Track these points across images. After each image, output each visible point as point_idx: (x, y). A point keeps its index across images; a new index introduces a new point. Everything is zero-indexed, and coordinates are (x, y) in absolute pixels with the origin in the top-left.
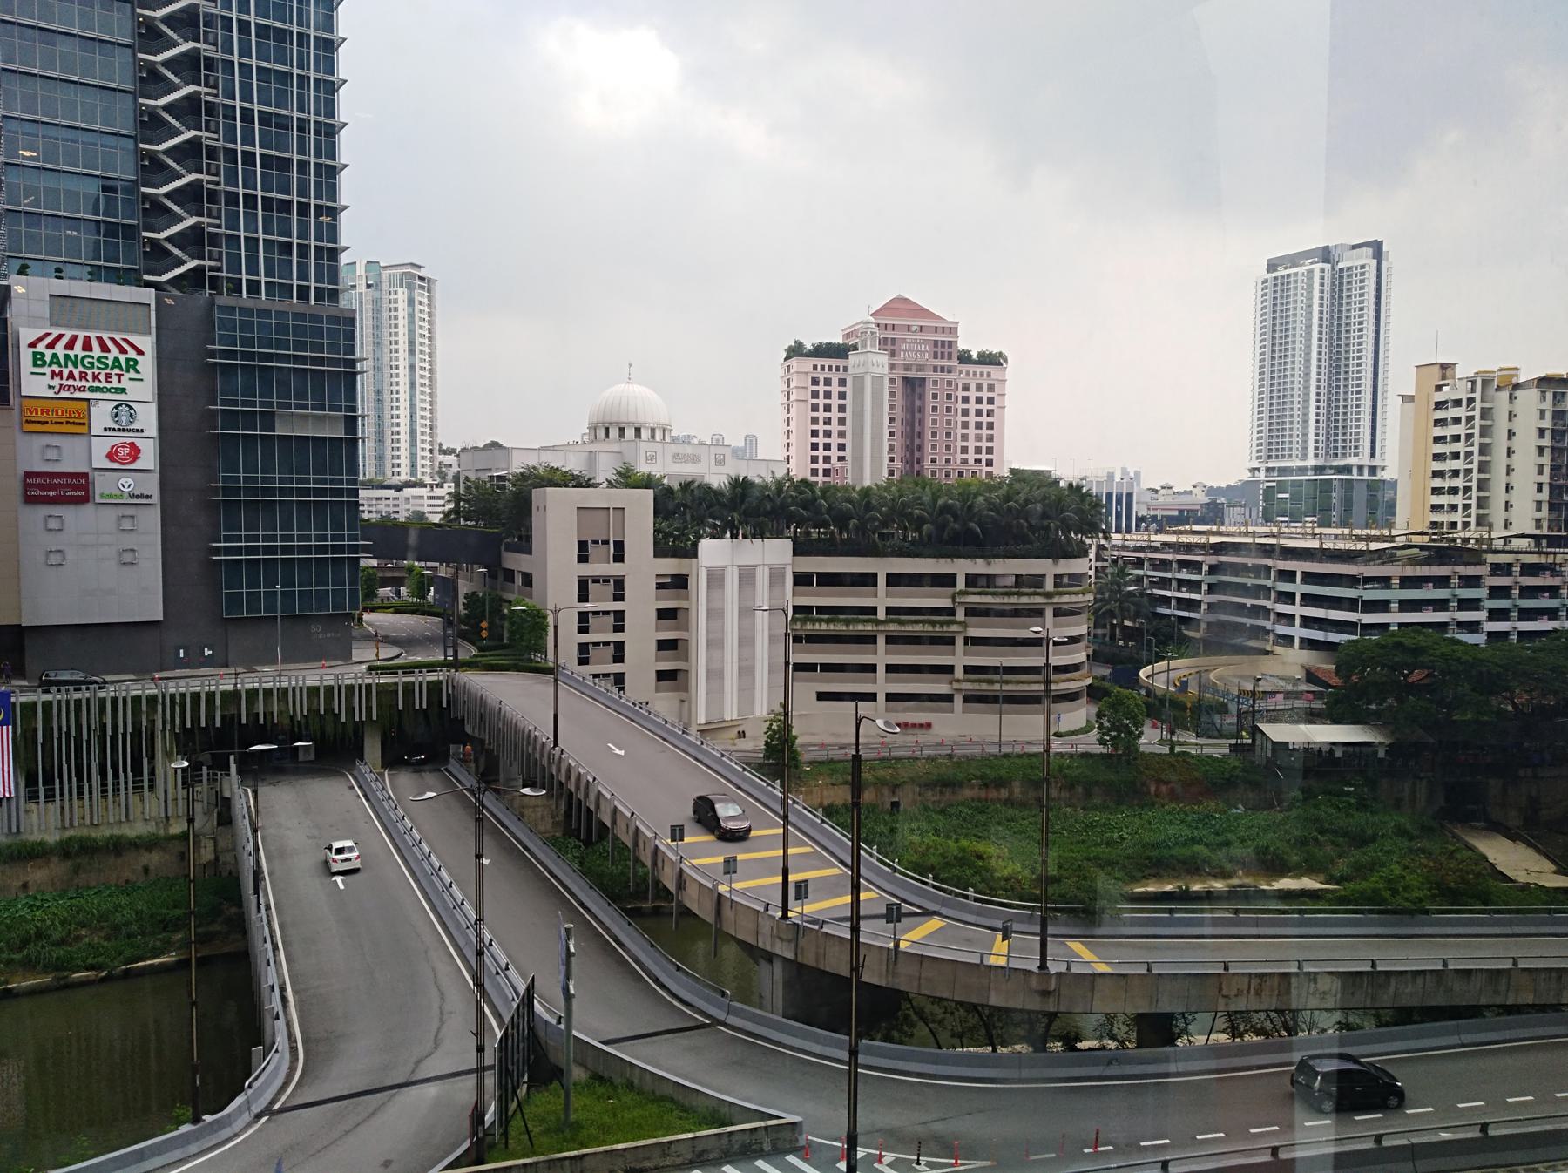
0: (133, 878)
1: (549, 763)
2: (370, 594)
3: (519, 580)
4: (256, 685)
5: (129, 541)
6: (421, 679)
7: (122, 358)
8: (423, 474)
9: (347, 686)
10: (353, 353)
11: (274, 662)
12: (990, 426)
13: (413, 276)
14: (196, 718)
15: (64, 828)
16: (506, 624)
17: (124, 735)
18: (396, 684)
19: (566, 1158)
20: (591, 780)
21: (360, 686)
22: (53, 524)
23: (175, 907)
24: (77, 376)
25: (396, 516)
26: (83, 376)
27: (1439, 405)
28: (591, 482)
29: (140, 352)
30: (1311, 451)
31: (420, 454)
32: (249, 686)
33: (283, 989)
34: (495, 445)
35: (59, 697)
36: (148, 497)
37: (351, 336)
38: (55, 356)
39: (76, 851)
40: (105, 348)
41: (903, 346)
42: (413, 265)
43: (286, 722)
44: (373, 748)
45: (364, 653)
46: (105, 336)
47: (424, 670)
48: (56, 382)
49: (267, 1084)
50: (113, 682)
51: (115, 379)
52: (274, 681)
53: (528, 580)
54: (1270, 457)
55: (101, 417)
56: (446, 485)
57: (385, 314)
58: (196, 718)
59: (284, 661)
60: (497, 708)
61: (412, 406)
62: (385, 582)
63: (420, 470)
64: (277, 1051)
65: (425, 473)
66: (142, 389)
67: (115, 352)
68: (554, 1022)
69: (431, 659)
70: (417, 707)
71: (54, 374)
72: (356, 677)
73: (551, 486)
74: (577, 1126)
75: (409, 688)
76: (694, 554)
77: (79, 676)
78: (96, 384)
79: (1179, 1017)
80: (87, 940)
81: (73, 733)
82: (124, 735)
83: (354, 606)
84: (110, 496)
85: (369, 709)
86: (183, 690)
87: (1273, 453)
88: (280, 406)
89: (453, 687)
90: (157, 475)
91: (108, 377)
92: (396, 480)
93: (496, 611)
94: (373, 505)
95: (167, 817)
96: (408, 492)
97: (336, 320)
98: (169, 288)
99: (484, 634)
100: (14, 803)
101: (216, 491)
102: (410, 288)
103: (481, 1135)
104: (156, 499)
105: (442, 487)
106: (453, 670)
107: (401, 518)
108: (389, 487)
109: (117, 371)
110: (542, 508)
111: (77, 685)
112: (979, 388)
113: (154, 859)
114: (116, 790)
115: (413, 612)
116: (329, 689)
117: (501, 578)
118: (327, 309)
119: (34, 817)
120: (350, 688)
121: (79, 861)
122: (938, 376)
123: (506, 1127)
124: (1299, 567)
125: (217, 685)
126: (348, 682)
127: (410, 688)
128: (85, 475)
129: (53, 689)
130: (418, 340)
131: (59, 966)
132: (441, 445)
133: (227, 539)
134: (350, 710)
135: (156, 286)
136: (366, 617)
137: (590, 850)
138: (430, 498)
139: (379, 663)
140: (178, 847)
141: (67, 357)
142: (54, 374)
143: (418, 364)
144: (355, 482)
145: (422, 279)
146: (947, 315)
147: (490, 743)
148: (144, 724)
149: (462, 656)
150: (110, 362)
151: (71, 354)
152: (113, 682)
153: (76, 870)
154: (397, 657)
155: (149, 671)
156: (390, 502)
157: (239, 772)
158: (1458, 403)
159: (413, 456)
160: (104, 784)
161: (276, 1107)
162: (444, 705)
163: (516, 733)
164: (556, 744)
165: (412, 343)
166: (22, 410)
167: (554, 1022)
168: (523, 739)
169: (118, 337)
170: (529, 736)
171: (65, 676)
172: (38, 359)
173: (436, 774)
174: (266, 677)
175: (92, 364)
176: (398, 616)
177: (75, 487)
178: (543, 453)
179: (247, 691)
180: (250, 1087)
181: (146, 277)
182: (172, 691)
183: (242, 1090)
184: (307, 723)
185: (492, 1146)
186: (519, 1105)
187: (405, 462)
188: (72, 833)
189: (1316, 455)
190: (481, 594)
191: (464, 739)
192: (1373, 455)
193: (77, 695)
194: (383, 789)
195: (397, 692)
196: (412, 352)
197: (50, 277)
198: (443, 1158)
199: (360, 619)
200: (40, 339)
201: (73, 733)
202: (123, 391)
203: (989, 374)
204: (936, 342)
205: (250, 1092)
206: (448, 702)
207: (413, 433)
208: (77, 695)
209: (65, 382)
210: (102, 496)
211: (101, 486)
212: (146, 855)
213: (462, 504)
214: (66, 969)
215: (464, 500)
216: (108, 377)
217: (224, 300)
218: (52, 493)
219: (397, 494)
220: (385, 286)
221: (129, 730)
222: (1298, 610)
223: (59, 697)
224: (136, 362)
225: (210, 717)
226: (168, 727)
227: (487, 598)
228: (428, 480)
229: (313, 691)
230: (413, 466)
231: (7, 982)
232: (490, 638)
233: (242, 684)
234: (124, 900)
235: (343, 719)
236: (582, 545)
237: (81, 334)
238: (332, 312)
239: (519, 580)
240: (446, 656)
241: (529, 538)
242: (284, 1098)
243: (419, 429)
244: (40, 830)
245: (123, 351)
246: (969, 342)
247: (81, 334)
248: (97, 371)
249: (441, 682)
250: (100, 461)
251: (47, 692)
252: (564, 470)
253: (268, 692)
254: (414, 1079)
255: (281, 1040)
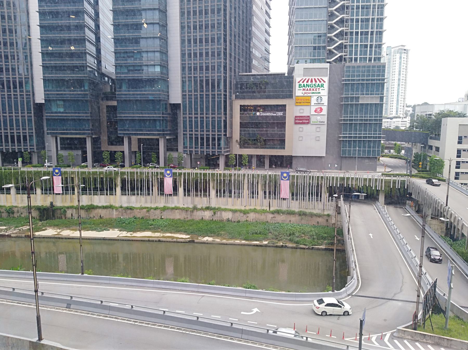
0: (315, 224)
1: (444, 211)
2: (383, 152)
3: (434, 149)
4: (349, 176)
5: (318, 134)
6: (399, 179)
7: (320, 84)
8: (400, 114)
9: (317, 176)
10: (384, 77)
11: (354, 170)
13: (402, 49)
14: (333, 184)
15: (34, 193)
16: (429, 164)
17: (315, 186)
18: (391, 180)
19: (445, 338)
20: (460, 219)
21: (379, 179)
22: (301, 130)
23: (325, 234)
24: (309, 90)
25: (390, 127)
26: (310, 90)
28: (465, 115)
29: (324, 82)
31: (399, 107)
32: (347, 176)
33: (355, 263)
34: (426, 104)
35: (300, 174)
36: (324, 122)
37: (384, 71)
38: (304, 85)
39: (302, 214)
40: (316, 81)
42: (402, 46)
43: (357, 188)
44: (382, 198)
45: (380, 170)
46: (316, 78)
47: (400, 176)
48: (304, 92)
49: (351, 287)
50: (312, 172)
51: (318, 90)
52: (354, 175)
53: (438, 149)
55: (314, 100)
56: (407, 117)
57: (392, 63)
58: (333, 184)
59: (358, 170)
60: (425, 191)
61: (398, 92)
62: (387, 148)
63: (399, 112)
64: (354, 279)
65: (401, 114)
66: (324, 92)
67: (318, 82)
68: (442, 295)
69: (401, 173)
70: (397, 187)
71: (303, 90)
72: (378, 177)
73: (449, 117)
74: (450, 330)
75: (394, 182)
77: (304, 169)
78: (313, 91)
79: (10, 345)
80: (304, 237)
81: (303, 184)
82: (315, 186)
83: (378, 155)
84: (315, 122)
85: (382, 186)
86: (330, 176)
88: (361, 94)
89: (409, 182)
90: (326, 116)
91: (316, 89)
92: (391, 116)
93: (425, 159)
94: (385, 124)
95: (324, 210)
96: (394, 120)
97: (379, 67)
98: (333, 63)
99: (420, 166)
100: (289, 200)
101: (341, 120)
102: (401, 53)
103: (416, 322)
104: (326, 123)
105: (406, 118)
106: (410, 177)
107: (392, 128)
108: (388, 118)
109: (318, 87)
110: (445, 125)
111: (305, 172)
113: (320, 220)
114: (312, 200)
115: (395, 158)
116: (370, 179)
117: (427, 148)
118: (377, 63)
119: (293, 204)
120: (376, 180)
121: (302, 217)
123: (425, 322)
125: (339, 175)
126: (376, 178)
127: (395, 181)
128: (309, 117)
129: (299, 172)
130: (402, 70)
131: (297, 243)
132: (407, 104)
133: (343, 134)
135: (329, 62)
136: (381, 159)
137: (455, 242)
138: (402, 122)
139: (385, 173)
140: (326, 218)
141: (307, 85)
142: (303, 90)
143: (401, 78)
144: (381, 117)
145: (405, 50)
147: (421, 202)
148: (320, 184)
149: (413, 173)
150: (317, 85)
151: (308, 84)
152: (312, 172)
153: (302, 219)
154: (390, 171)
155: (321, 170)
156: (389, 123)
157: (344, 200)
159: (397, 108)
160: (309, 198)
161: (353, 294)
162: (406, 188)
163: (431, 200)
164: (447, 205)
165: (400, 71)
166: (296, 99)
167: (442, 295)
168: (434, 202)
169: (319, 78)
170: (436, 201)
171: (301, 169)
172: (300, 86)
173: (402, 209)
174: (351, 174)
175: (312, 86)
176: (391, 159)
177: (306, 120)
178: (447, 106)
179: (347, 178)
180: (347, 286)
181: (327, 60)
182: (327, 175)
183: (344, 287)
184: (363, 188)
185: (419, 326)
186: (430, 317)
187: (394, 110)
188: (301, 210)
190: (420, 153)
191: (411, 199)
193: (304, 174)
194: (385, 211)
195: (391, 182)
196: (400, 74)
197: (303, 63)
198: (404, 324)
199: (379, 159)
200: (301, 80)
201: (303, 184)
202: (320, 93)
205: (347, 288)
206: (407, 187)
207: (398, 101)
208: (304, 174)
209: (306, 92)
210: (313, 122)
211: (313, 119)
212: (318, 218)
213: (415, 123)
214: (299, 244)
215: (416, 122)
216: (316, 89)
217: (348, 64)
218: (301, 121)
219: (391, 121)
220: (392, 54)
221: (316, 185)
223: (300, 174)
224: (323, 85)
225: (336, 184)
226: (326, 185)
227: (422, 154)
228: (401, 116)
229: (365, 180)
230: (397, 111)
231: (286, 244)
232: (422, 168)
233: (346, 175)
234: (313, 229)
235: (374, 189)
236: (460, 138)
237: (313, 78)
238: (379, 64)
239: (434, 149)
240: (407, 173)
241: (439, 135)
242: (355, 292)
243: (400, 99)
244: (294, 208)
245: (320, 82)
247: (310, 78)
248: (313, 88)
249: (405, 181)
250: (313, 113)
251: (297, 173)
252: (455, 111)
253: (352, 178)
254: (394, 299)
255: (355, 276)
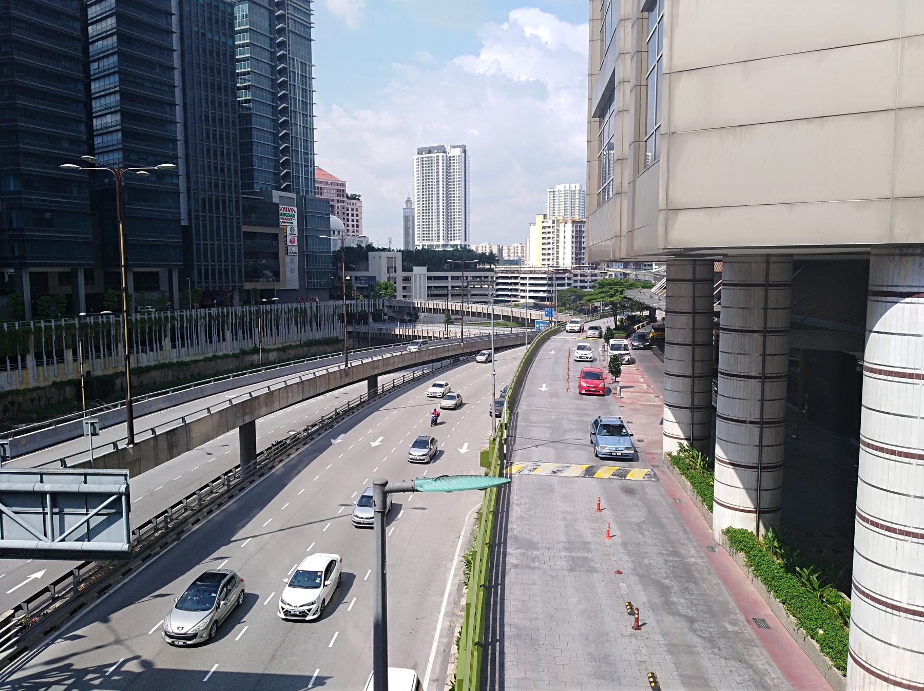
12: (357, 226)
27: (544, 227)
30: (441, 238)
41: (325, 191)
54: (424, 240)
76: (412, 270)
87: (425, 238)
112: (353, 210)
122: (339, 204)
124: (528, 276)
134: (351, 311)
146: (341, 178)
158: (549, 227)
189: (443, 239)
192: (465, 240)
203: (356, 204)
204: (338, 189)
222: (528, 288)
246: (349, 191)
